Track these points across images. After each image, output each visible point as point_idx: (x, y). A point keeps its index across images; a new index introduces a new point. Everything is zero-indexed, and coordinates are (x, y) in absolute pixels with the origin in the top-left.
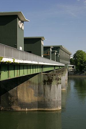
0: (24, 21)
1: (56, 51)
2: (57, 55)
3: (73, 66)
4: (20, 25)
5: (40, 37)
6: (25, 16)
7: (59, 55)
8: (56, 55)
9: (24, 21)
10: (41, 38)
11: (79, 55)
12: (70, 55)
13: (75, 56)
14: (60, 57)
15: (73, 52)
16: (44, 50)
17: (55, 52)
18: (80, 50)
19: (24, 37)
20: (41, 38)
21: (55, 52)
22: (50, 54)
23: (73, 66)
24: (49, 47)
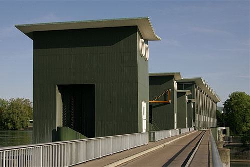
0: (148, 40)
1: (188, 92)
2: (189, 102)
3: (224, 128)
4: (143, 48)
5: (132, 20)
6: (157, 28)
7: (194, 103)
8: (188, 103)
9: (148, 40)
10: (136, 27)
11: (235, 102)
12: (216, 103)
13: (228, 105)
14: (196, 109)
15: (223, 97)
16: (34, 49)
17: (184, 93)
18: (240, 91)
19: (149, 72)
20: (136, 27)
21: (184, 93)
22: (172, 99)
23: (224, 128)
24: (169, 78)
